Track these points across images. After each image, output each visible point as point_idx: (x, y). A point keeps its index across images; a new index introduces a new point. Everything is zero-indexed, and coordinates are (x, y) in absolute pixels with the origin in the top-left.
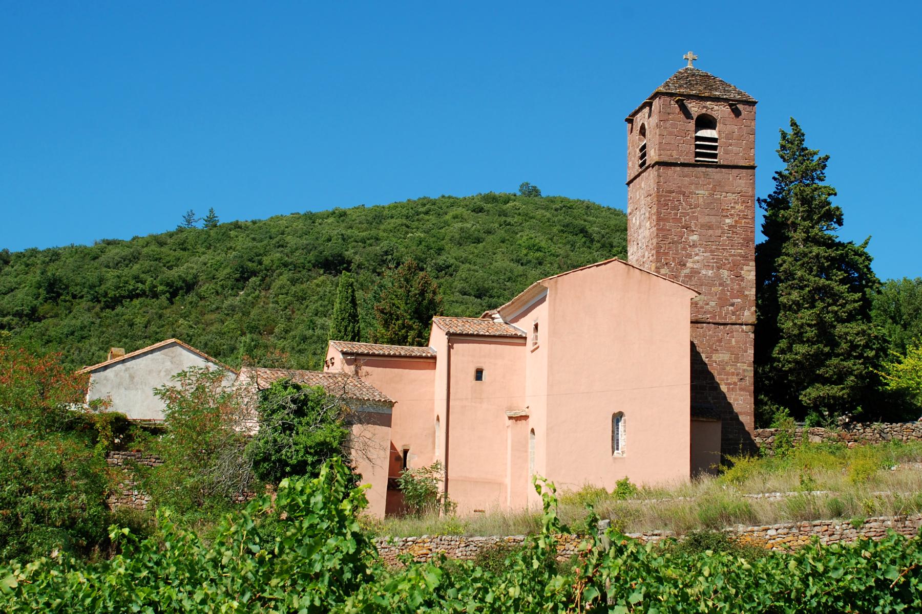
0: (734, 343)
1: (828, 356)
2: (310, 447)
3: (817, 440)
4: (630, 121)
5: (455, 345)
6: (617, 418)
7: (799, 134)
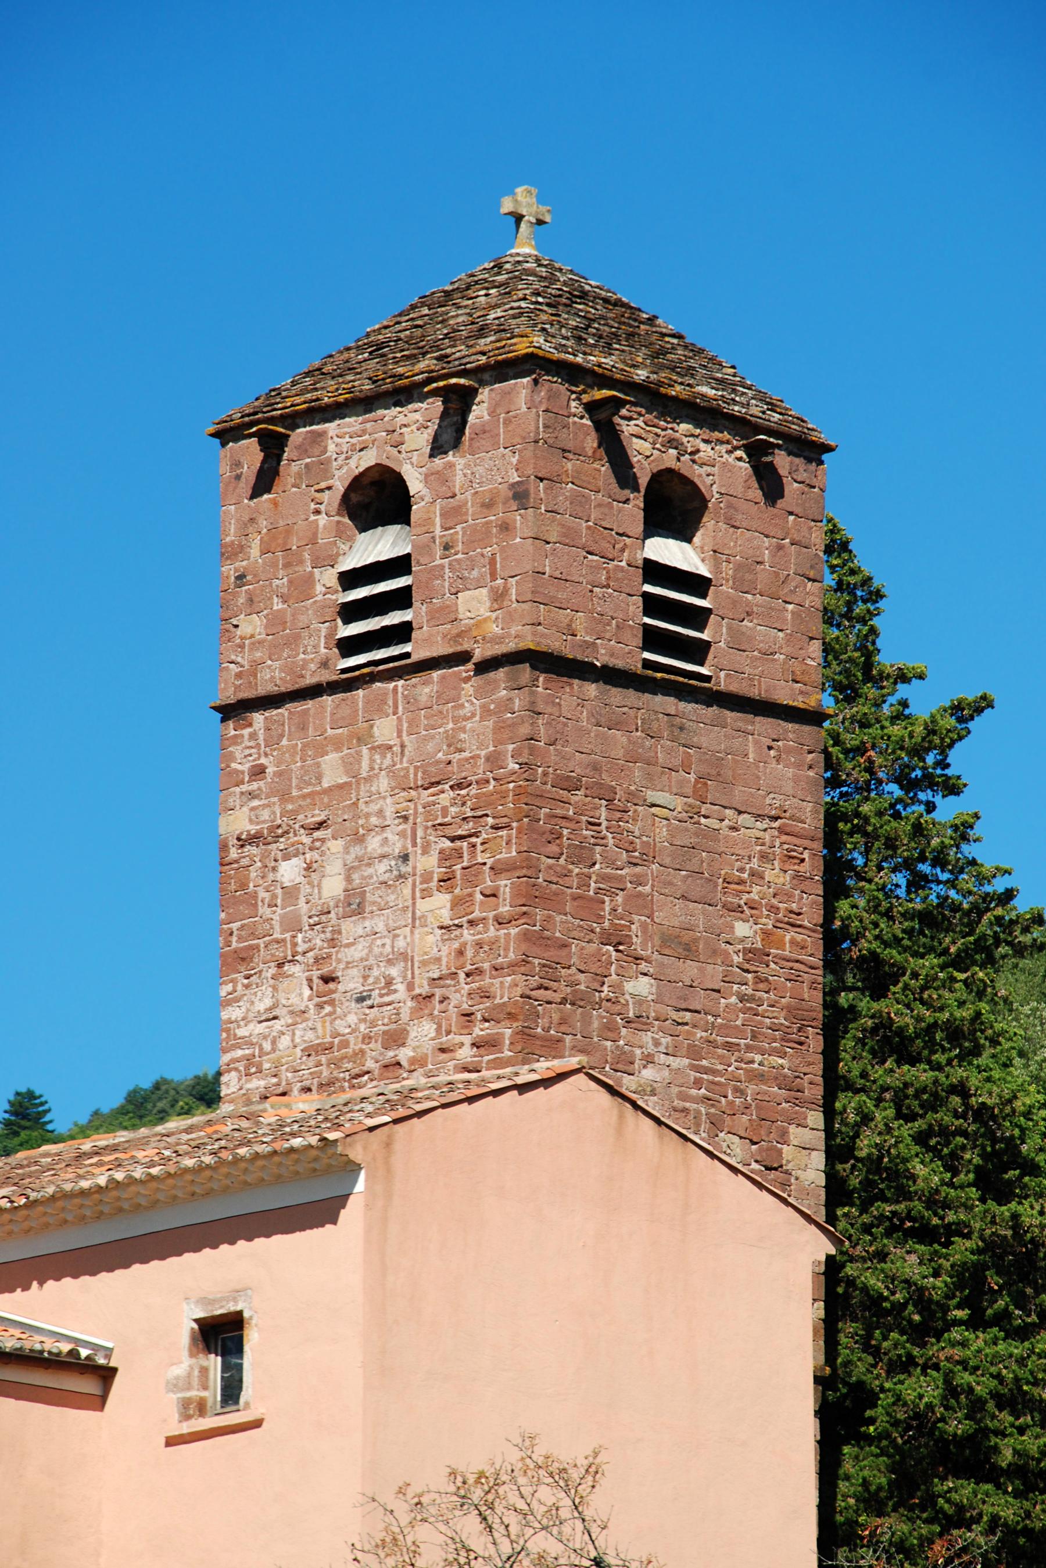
4: (270, 433)
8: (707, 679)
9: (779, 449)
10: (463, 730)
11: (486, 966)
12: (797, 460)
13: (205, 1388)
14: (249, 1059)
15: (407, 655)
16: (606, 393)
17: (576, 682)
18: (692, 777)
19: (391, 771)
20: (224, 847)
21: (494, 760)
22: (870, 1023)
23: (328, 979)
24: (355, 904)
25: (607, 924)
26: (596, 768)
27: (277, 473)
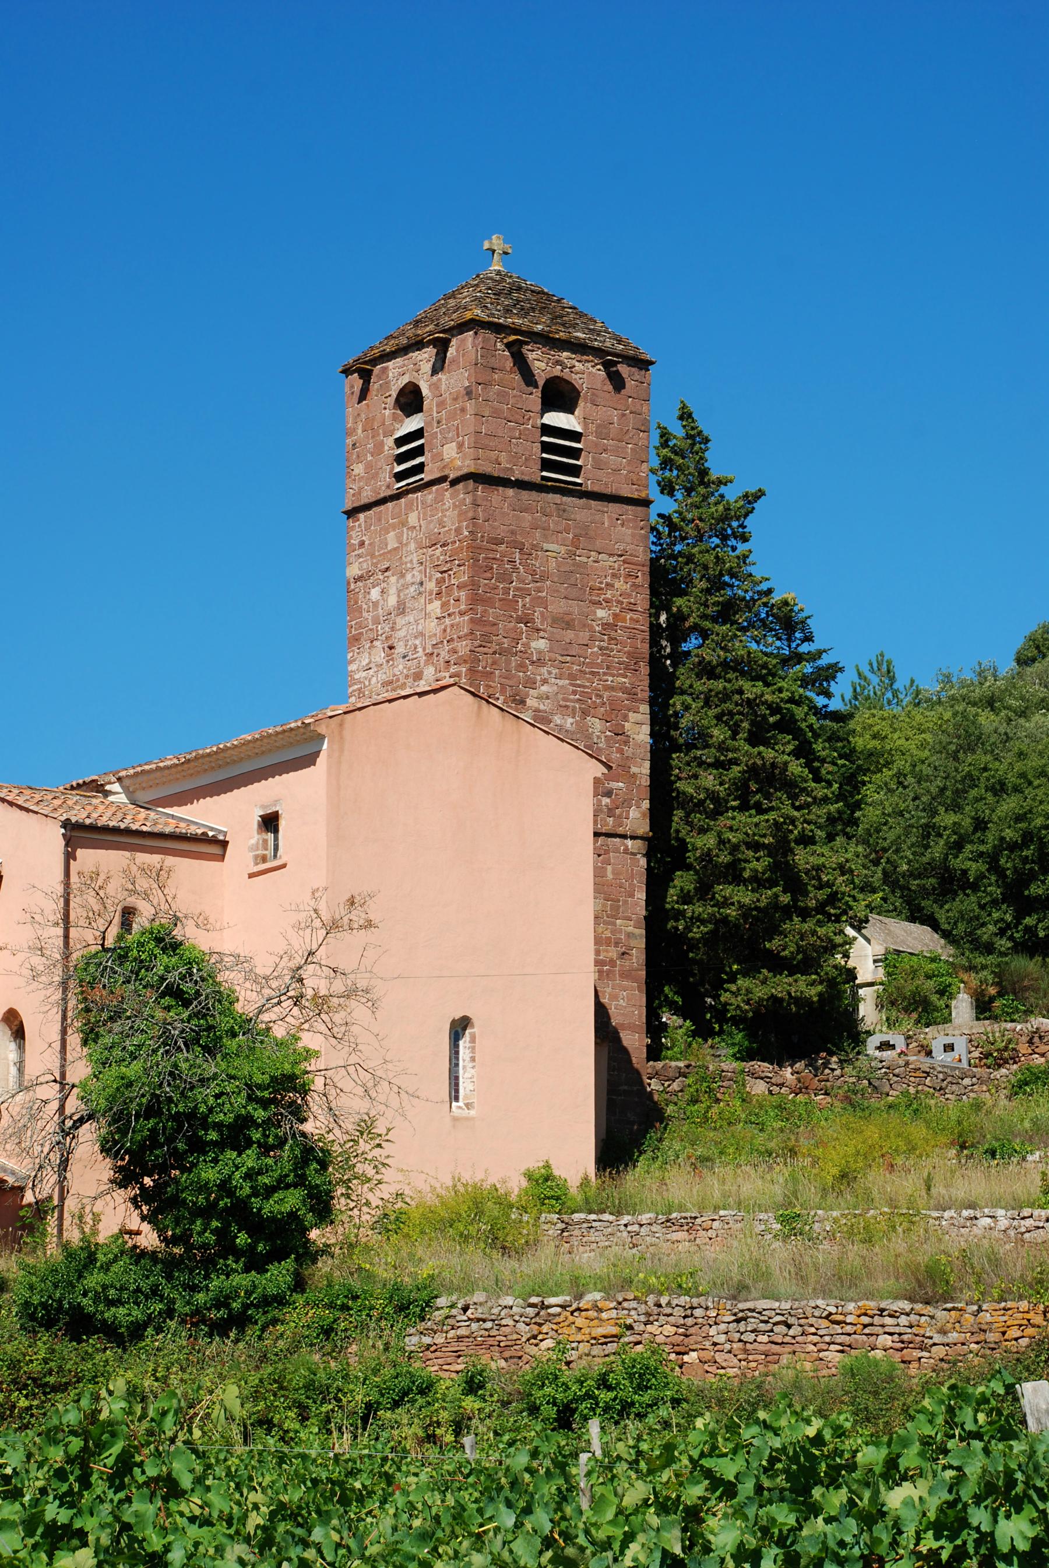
0: (610, 876)
1: (787, 912)
2: (259, 1087)
3: (759, 1088)
4: (364, 370)
5: (80, 852)
6: (460, 1027)
7: (697, 439)
8: (580, 485)
9: (621, 364)
10: (445, 516)
11: (455, 636)
12: (633, 369)
13: (266, 849)
14: (359, 689)
15: (422, 479)
16: (513, 338)
17: (501, 488)
18: (571, 536)
19: (415, 539)
20: (349, 583)
21: (458, 531)
22: (697, 660)
23: (391, 648)
24: (401, 609)
25: (520, 613)
26: (513, 532)
27: (368, 390)
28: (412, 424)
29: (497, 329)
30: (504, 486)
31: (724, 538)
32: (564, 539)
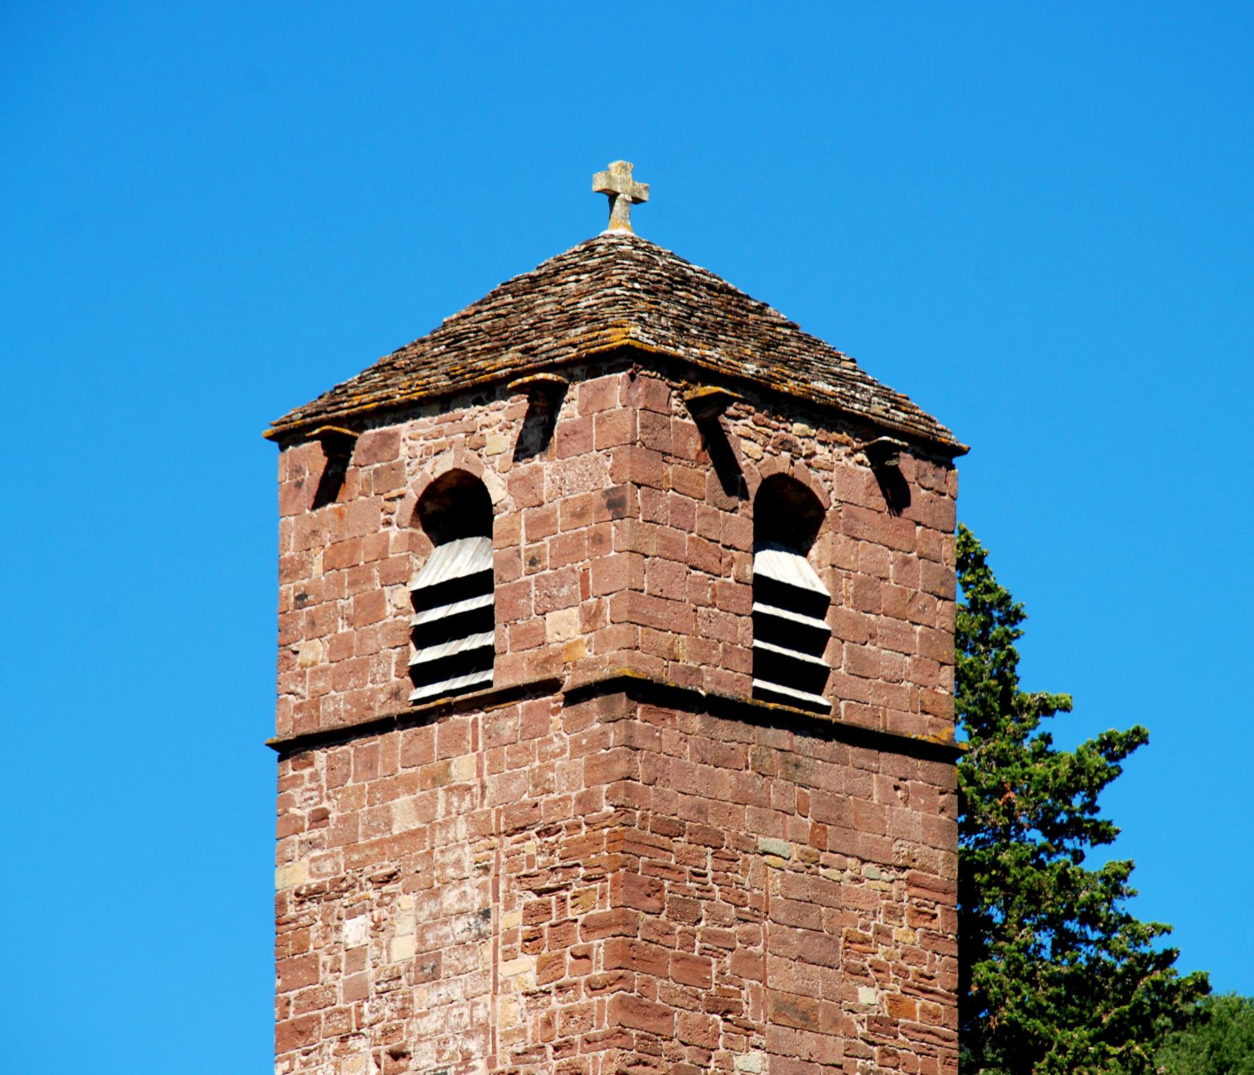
4: (334, 436)
8: (826, 710)
9: (903, 451)
11: (577, 1038)
12: (925, 464)
15: (488, 684)
16: (711, 389)
17: (678, 713)
18: (809, 821)
19: (470, 816)
20: (281, 904)
21: (586, 802)
24: (428, 968)
25: (713, 989)
26: (701, 810)
28: (460, 559)
29: (673, 368)
30: (686, 709)
31: (1055, 832)
32: (797, 828)
